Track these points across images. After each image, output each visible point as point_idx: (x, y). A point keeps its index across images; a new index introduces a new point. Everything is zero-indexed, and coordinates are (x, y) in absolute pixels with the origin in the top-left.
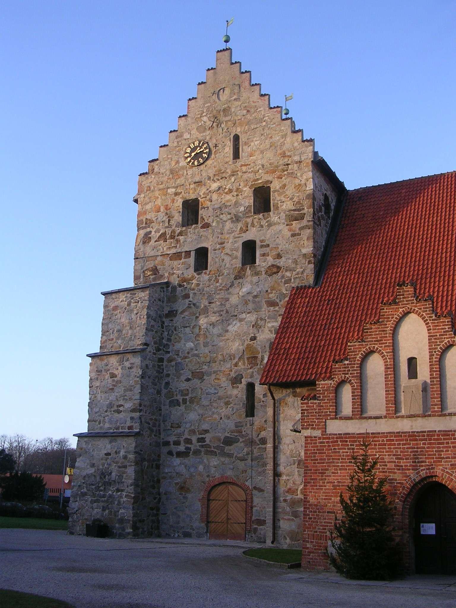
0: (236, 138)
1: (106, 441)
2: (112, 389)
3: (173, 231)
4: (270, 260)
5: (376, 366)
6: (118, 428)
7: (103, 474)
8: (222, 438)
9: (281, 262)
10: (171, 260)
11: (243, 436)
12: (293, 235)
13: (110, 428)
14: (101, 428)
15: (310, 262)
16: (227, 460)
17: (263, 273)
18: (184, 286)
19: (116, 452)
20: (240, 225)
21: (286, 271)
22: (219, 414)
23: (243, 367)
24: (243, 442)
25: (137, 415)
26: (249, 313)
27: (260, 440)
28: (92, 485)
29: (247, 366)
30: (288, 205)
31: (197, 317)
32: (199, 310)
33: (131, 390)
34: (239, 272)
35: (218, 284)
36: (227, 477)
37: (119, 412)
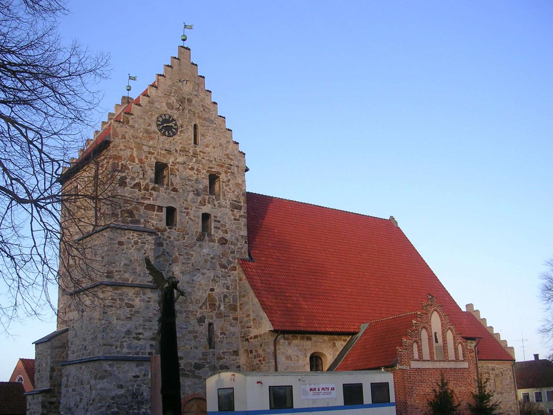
0: (195, 126)
1: (133, 364)
2: (130, 318)
3: (147, 185)
4: (220, 234)
5: (424, 334)
6: (137, 353)
7: (134, 394)
8: (193, 363)
9: (228, 237)
10: (145, 209)
11: (208, 363)
12: (235, 219)
13: (130, 353)
14: (118, 352)
15: (245, 242)
16: (197, 381)
17: (217, 241)
18: (158, 235)
19: (144, 375)
20: (200, 199)
21: (232, 244)
22: (190, 345)
23: (205, 310)
24: (209, 367)
25: (153, 343)
26: (208, 270)
27: (220, 366)
28: (125, 404)
29: (209, 310)
30: (231, 196)
31: (170, 264)
32: (171, 258)
33: (150, 321)
34: (200, 236)
35: (184, 241)
36: (197, 394)
37: (139, 339)
